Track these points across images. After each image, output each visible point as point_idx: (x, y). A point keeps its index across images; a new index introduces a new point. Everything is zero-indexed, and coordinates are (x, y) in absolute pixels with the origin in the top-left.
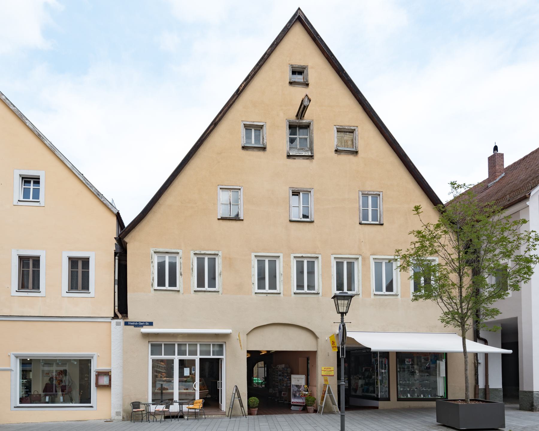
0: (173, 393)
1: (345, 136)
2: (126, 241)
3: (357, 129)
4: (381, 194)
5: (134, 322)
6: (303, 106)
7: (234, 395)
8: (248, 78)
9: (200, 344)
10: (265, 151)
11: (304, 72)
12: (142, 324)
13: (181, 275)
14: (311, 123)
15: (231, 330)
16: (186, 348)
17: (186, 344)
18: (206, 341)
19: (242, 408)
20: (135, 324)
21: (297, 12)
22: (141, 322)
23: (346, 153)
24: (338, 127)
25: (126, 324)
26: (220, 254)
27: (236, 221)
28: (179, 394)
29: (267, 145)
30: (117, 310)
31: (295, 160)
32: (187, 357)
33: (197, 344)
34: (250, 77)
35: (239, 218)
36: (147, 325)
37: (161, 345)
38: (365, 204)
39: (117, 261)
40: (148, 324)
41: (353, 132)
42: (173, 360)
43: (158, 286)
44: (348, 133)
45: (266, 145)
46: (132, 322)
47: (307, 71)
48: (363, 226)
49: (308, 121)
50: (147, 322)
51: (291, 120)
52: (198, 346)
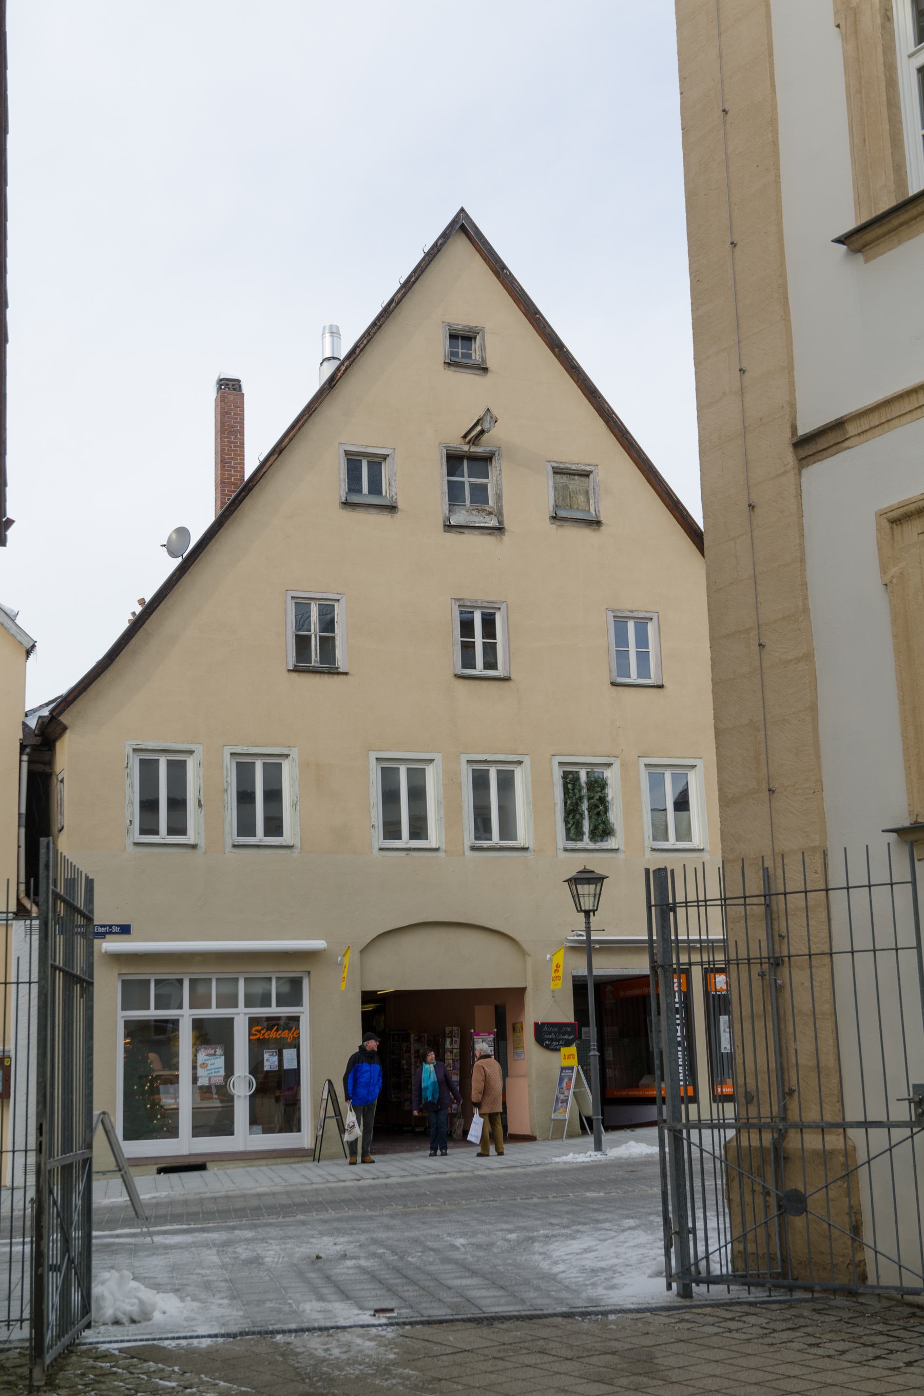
0: (178, 1109)
1: (572, 482)
4: (655, 616)
6: (479, 428)
7: (324, 1103)
11: (475, 338)
12: (103, 930)
13: (200, 805)
14: (497, 454)
15: (324, 942)
16: (271, 985)
21: (457, 215)
23: (575, 524)
24: (555, 465)
26: (294, 753)
31: (462, 536)
32: (214, 1012)
33: (237, 980)
34: (358, 350)
36: (115, 933)
38: (621, 638)
39: (25, 766)
40: (117, 929)
42: (178, 1021)
44: (576, 477)
45: (396, 499)
47: (483, 339)
48: (619, 688)
49: (490, 449)
50: (116, 925)
52: (241, 984)
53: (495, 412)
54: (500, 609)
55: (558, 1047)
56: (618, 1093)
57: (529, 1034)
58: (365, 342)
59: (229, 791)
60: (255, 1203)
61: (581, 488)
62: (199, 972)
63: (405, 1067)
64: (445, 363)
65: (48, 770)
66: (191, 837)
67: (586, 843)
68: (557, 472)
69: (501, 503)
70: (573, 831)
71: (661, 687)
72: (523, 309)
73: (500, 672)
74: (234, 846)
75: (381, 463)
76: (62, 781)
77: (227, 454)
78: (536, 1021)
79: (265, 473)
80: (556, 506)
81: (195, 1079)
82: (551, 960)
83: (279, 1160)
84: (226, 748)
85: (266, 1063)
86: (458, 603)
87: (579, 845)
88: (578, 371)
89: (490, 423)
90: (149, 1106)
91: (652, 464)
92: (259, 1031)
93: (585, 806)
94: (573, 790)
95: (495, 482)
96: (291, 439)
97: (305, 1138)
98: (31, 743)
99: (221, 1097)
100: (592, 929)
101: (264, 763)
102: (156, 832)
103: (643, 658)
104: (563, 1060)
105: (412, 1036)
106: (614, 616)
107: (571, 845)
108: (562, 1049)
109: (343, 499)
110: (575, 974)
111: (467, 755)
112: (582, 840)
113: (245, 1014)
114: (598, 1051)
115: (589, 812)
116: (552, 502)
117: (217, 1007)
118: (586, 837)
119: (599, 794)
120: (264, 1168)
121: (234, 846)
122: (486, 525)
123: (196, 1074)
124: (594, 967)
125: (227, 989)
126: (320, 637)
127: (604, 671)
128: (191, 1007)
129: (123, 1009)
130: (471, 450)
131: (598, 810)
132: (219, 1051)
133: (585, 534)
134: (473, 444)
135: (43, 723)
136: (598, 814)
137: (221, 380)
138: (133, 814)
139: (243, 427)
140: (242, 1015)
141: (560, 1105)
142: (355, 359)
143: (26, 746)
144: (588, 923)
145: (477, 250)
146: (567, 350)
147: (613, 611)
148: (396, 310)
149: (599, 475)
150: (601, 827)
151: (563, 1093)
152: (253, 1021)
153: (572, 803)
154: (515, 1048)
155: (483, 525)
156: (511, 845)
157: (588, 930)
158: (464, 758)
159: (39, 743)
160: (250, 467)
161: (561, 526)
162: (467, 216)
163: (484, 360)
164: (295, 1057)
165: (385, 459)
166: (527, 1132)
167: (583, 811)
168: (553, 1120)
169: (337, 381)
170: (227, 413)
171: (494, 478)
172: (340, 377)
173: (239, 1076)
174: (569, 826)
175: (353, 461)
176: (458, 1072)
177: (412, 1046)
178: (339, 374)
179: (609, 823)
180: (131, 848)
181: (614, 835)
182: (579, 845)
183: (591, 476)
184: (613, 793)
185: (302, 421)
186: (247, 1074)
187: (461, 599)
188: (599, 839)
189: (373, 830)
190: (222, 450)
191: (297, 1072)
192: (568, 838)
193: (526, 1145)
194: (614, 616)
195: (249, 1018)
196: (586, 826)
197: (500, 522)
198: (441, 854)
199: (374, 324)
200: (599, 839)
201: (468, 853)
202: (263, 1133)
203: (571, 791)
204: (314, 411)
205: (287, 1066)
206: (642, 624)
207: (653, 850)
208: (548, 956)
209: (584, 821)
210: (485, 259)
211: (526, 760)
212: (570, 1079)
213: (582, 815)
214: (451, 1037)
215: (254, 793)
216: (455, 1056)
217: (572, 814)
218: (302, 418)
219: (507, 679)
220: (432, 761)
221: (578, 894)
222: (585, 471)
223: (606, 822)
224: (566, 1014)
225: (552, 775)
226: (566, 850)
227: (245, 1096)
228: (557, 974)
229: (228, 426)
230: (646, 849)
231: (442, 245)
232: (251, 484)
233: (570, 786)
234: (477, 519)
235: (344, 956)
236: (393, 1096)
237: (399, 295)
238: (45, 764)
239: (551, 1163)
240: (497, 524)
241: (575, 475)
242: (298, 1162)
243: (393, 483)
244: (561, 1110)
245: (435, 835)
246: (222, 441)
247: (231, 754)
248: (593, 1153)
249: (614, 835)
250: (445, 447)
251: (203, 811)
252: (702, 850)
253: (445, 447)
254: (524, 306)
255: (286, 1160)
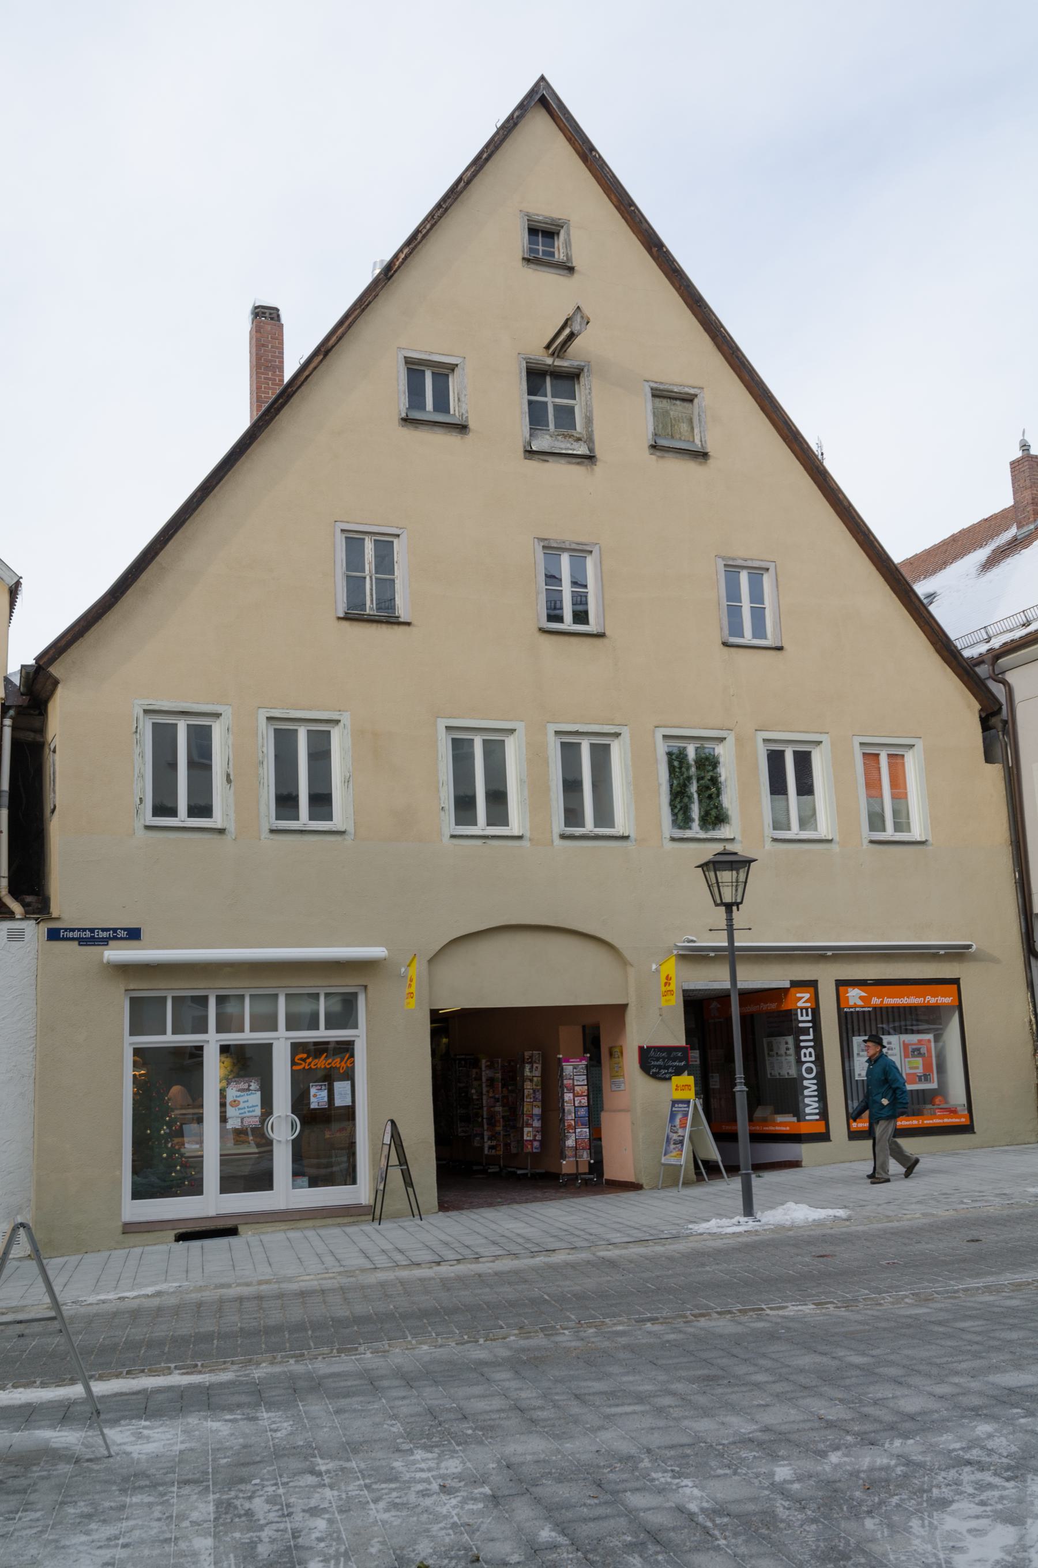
0: (202, 1156)
1: (673, 408)
2: (55, 675)
3: (702, 395)
4: (772, 566)
5: (79, 930)
6: (567, 331)
7: (386, 1148)
8: (416, 239)
9: (287, 995)
10: (465, 434)
11: (558, 234)
12: (105, 934)
13: (229, 780)
14: (586, 370)
15: (384, 949)
16: (318, 1005)
17: (242, 997)
18: (305, 985)
19: (410, 1190)
20: (83, 935)
21: (537, 84)
22: (104, 930)
23: (678, 455)
25: (54, 935)
26: (346, 718)
27: (390, 626)
28: (221, 1161)
29: (470, 418)
30: (7, 890)
31: (546, 465)
32: (247, 1036)
33: (276, 996)
34: (420, 236)
35: (398, 617)
36: (121, 939)
37: (164, 999)
38: (733, 593)
40: (124, 934)
41: (691, 401)
43: (153, 816)
44: (678, 402)
45: (467, 417)
46: (73, 930)
47: (569, 235)
48: (733, 650)
50: (121, 929)
51: (532, 357)
53: (587, 311)
54: (591, 552)
55: (667, 1076)
56: (728, 1128)
57: (631, 1060)
58: (428, 226)
59: (265, 763)
60: (296, 1313)
61: (684, 415)
62: (228, 986)
63: (475, 1097)
64: (524, 259)
65: (39, 739)
66: (217, 820)
67: (696, 830)
68: (658, 394)
69: (592, 427)
70: (680, 817)
71: (780, 649)
72: (614, 200)
73: (592, 627)
74: (272, 831)
75: (447, 376)
76: (54, 751)
77: (264, 393)
78: (641, 1045)
79: (308, 377)
80: (656, 435)
81: (224, 1119)
82: (658, 971)
83: (329, 1221)
84: (261, 711)
85: (312, 1099)
86: (542, 544)
87: (688, 834)
88: (680, 275)
89: (581, 325)
90: (165, 1155)
91: (768, 389)
92: (304, 1060)
93: (694, 788)
94: (680, 768)
95: (583, 403)
96: (340, 339)
97: (361, 1192)
98: (15, 703)
99: (258, 1140)
100: (735, 927)
101: (308, 731)
102: (173, 812)
103: (758, 615)
104: (674, 1091)
105: (484, 1061)
106: (725, 565)
107: (679, 833)
108: (673, 1078)
109: (404, 415)
110: (686, 987)
111: (556, 725)
112: (690, 828)
113: (287, 1039)
114: (745, 1084)
115: (699, 795)
116: (651, 429)
117: (252, 1030)
118: (696, 825)
119: (711, 774)
120: (310, 1234)
121: (272, 831)
122: (575, 452)
123: (225, 1112)
124: (738, 978)
125: (264, 1008)
126: (376, 579)
127: (715, 629)
128: (218, 1031)
129: (131, 1034)
130: (556, 364)
131: (709, 792)
132: (254, 1086)
133: (691, 467)
134: (558, 356)
135: (28, 674)
136: (710, 797)
137: (256, 308)
138: (144, 792)
139: (282, 362)
140: (282, 1040)
141: (672, 1146)
142: (416, 246)
143: (9, 708)
144: (730, 920)
145: (560, 129)
146: (667, 250)
147: (723, 558)
148: (465, 192)
149: (705, 400)
150: (714, 813)
151: (676, 1133)
152: (296, 1048)
153: (679, 784)
154: (612, 1077)
155: (570, 452)
156: (608, 833)
157: (730, 929)
158: (552, 728)
159: (25, 704)
160: (290, 369)
161: (663, 457)
162: (548, 86)
163: (569, 258)
164: (349, 1092)
165: (453, 370)
166: (631, 1178)
167: (692, 794)
168: (664, 1165)
169: (395, 271)
170: (263, 345)
171: (583, 398)
172: (399, 267)
173: (279, 1117)
174: (676, 811)
175: (415, 369)
176: (539, 1104)
177: (483, 1073)
178: (397, 263)
179: (722, 808)
180: (141, 833)
181: (728, 823)
182: (688, 834)
183: (696, 401)
184: (725, 772)
185: (353, 316)
186: (289, 1113)
187: (546, 539)
188: (711, 827)
189: (442, 813)
190: (258, 388)
191: (350, 1113)
192: (675, 823)
193: (631, 1195)
194: (725, 565)
195: (292, 1043)
196: (695, 812)
197: (591, 450)
198: (525, 843)
199: (439, 206)
200: (711, 827)
201: (557, 841)
202: (310, 1186)
203: (677, 770)
204: (368, 305)
205: (338, 1102)
206: (757, 573)
207: (775, 840)
208: (654, 967)
209: (692, 806)
210: (569, 140)
211: (625, 731)
212: (686, 1115)
213: (690, 797)
214: (531, 1063)
215: (297, 796)
216: (537, 1085)
217: (679, 796)
218: (353, 313)
219: (601, 635)
220: (512, 731)
221: (718, 883)
222: (688, 394)
223: (719, 807)
224: (675, 1035)
225: (655, 750)
226: (673, 839)
227: (287, 1141)
228: (668, 988)
229: (267, 361)
230: (766, 839)
231: (521, 117)
232: (290, 390)
233: (676, 763)
234: (563, 446)
235: (409, 966)
236: (460, 1130)
237: (469, 174)
238: (35, 731)
239: (691, 1235)
240: (588, 453)
241: (676, 399)
242: (354, 1223)
243: (463, 399)
244: (674, 1154)
245: (517, 821)
246: (258, 377)
247: (267, 718)
248: (743, 1219)
249: (728, 823)
250: (524, 359)
251: (232, 788)
252: (830, 841)
253: (524, 359)
254: (616, 196)
255: (339, 1220)
